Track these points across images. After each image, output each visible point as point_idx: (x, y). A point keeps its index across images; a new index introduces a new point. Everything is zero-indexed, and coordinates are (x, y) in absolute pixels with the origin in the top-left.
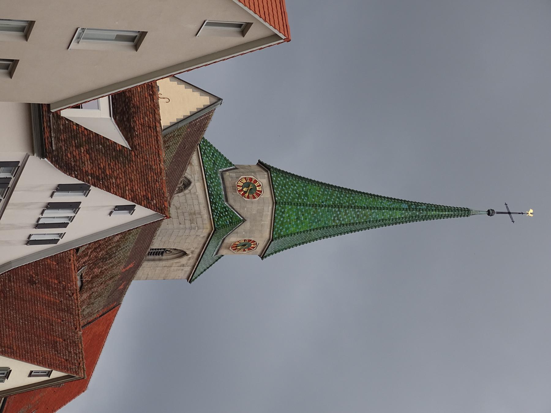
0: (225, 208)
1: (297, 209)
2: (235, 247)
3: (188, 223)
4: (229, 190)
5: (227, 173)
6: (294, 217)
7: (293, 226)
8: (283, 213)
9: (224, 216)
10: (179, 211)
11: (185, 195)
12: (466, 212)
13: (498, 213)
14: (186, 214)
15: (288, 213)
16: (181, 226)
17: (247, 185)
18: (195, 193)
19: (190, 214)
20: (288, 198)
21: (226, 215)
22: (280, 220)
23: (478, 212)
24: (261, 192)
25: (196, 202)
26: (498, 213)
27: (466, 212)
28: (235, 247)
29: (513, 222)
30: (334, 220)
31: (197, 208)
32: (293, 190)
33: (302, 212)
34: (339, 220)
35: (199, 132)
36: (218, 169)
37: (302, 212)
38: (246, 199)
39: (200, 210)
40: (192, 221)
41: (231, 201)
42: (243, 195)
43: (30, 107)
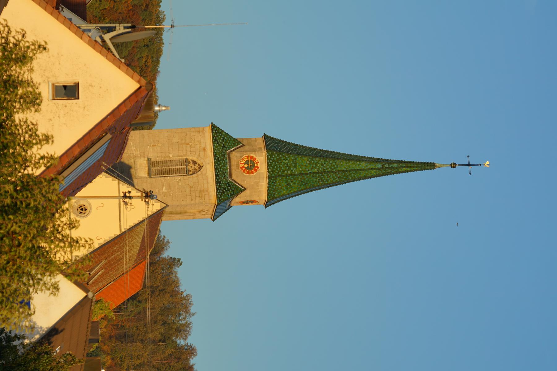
0: (228, 183)
1: (286, 179)
2: (237, 203)
3: (198, 200)
4: (233, 168)
5: (234, 153)
6: (284, 184)
7: (284, 190)
8: (275, 183)
9: (227, 191)
10: (192, 189)
11: (198, 176)
12: (431, 166)
13: (459, 165)
14: (197, 192)
15: (279, 182)
16: (193, 202)
17: (247, 162)
18: (205, 174)
19: (201, 191)
20: (279, 171)
21: (229, 190)
22: (273, 188)
23: (443, 165)
24: (258, 167)
25: (205, 182)
26: (459, 165)
27: (431, 166)
28: (237, 203)
29: (470, 173)
30: (319, 182)
31: (206, 186)
32: (285, 163)
33: (291, 180)
34: (323, 181)
35: (192, 217)
36: (226, 151)
37: (291, 180)
38: (246, 175)
39: (208, 187)
40: (201, 197)
41: (234, 177)
42: (244, 171)
43: (77, 86)
